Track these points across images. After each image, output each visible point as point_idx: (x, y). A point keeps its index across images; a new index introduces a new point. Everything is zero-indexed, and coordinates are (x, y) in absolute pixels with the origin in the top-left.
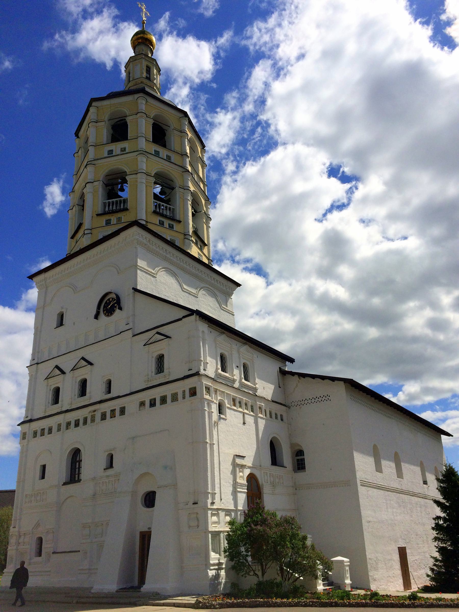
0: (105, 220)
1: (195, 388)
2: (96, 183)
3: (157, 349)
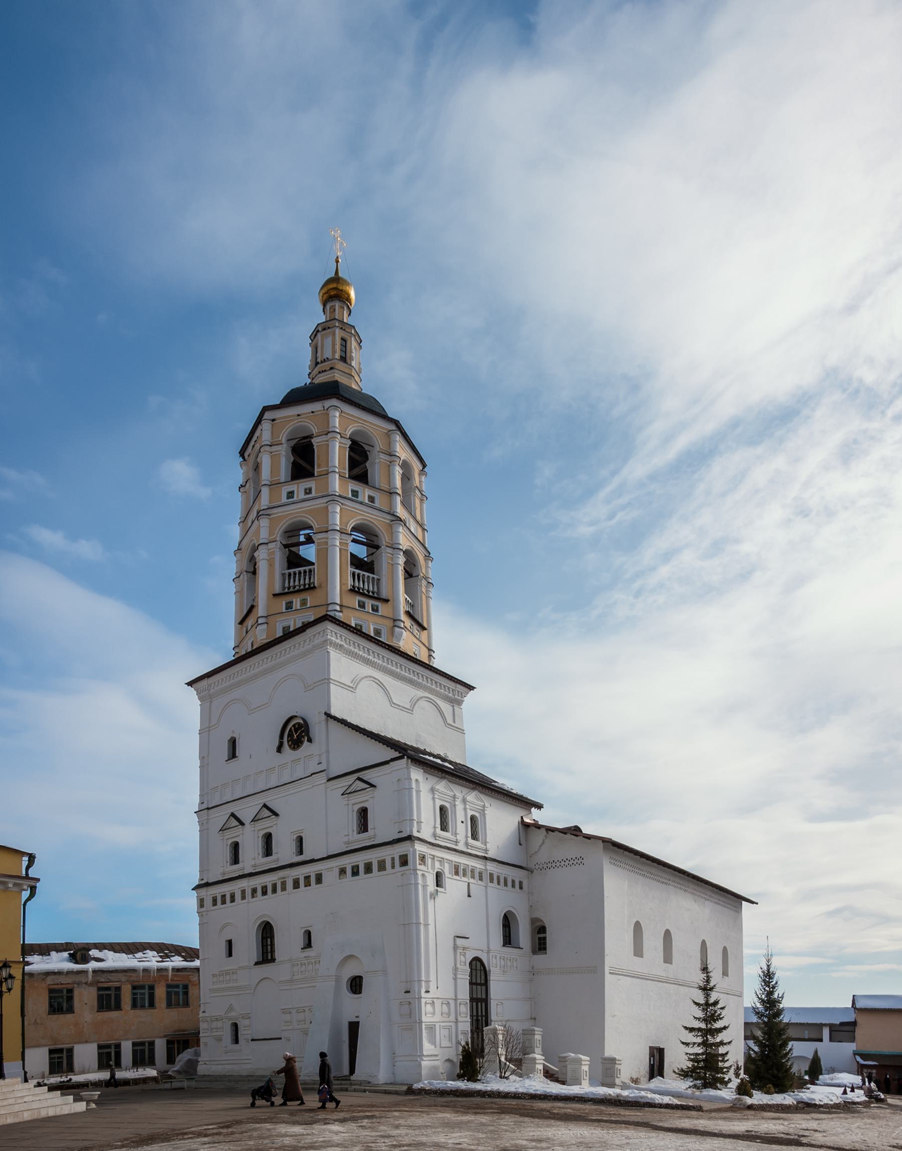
0: (284, 603)
1: (406, 856)
2: (271, 546)
3: (359, 800)
